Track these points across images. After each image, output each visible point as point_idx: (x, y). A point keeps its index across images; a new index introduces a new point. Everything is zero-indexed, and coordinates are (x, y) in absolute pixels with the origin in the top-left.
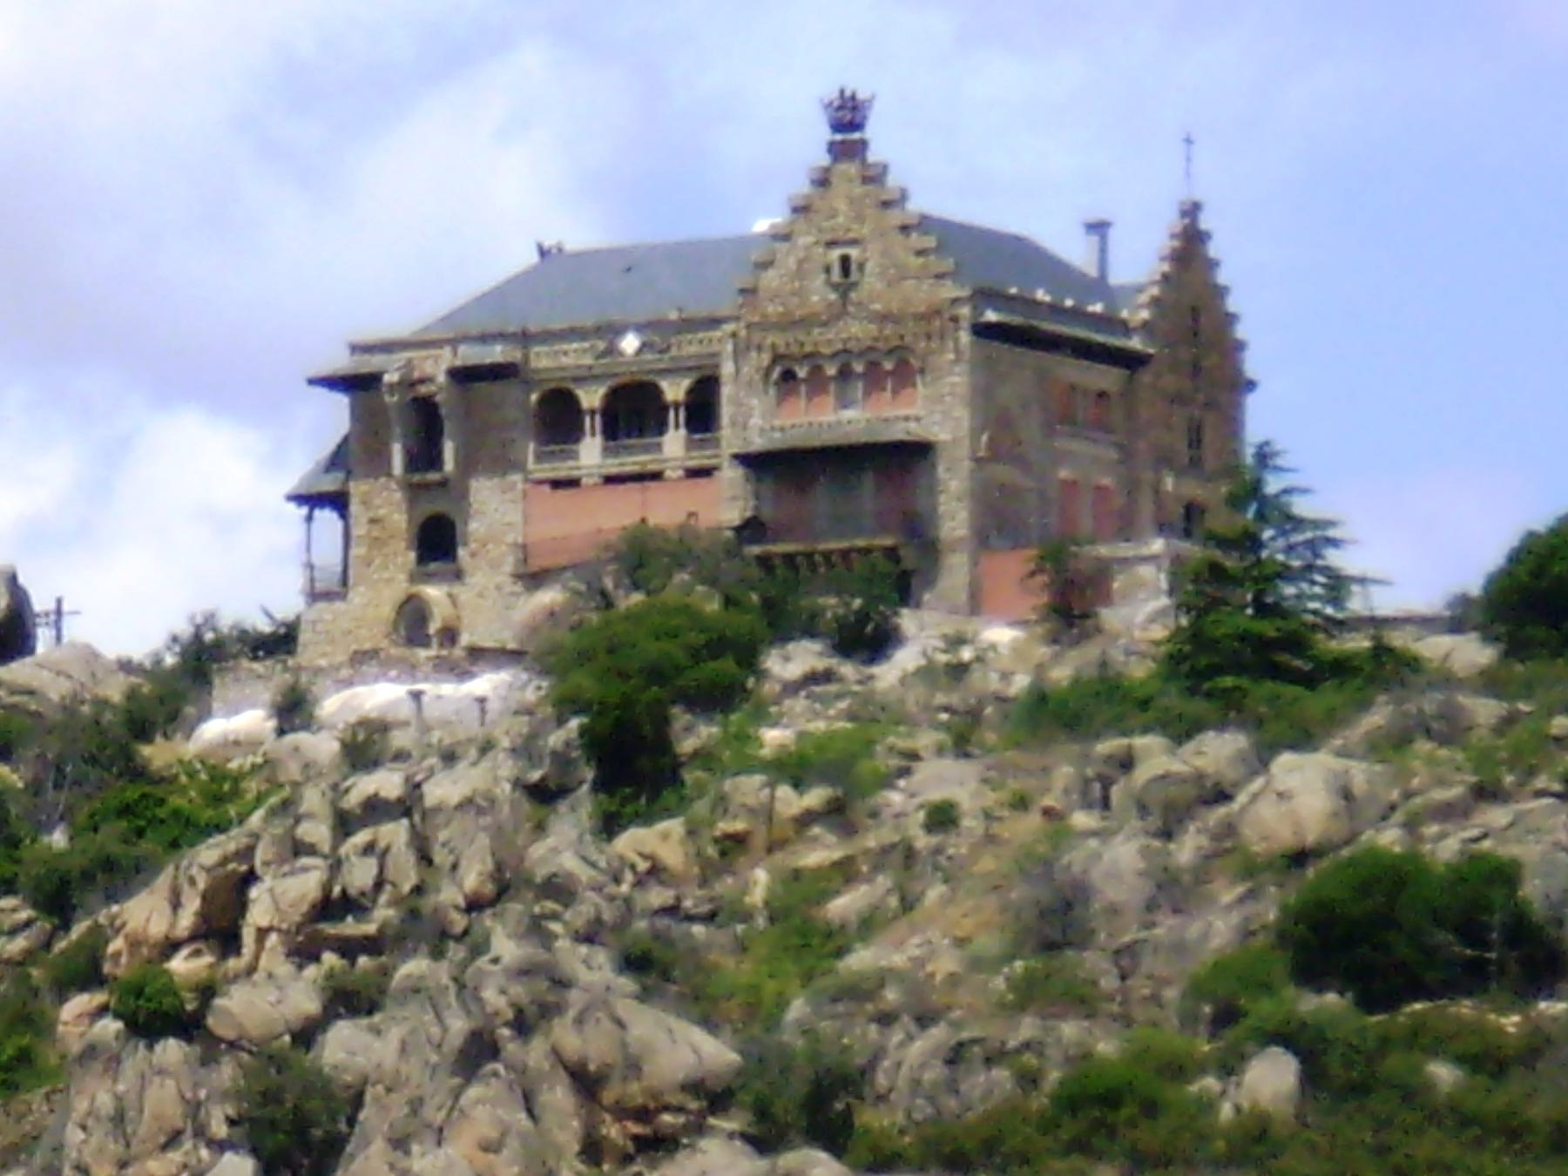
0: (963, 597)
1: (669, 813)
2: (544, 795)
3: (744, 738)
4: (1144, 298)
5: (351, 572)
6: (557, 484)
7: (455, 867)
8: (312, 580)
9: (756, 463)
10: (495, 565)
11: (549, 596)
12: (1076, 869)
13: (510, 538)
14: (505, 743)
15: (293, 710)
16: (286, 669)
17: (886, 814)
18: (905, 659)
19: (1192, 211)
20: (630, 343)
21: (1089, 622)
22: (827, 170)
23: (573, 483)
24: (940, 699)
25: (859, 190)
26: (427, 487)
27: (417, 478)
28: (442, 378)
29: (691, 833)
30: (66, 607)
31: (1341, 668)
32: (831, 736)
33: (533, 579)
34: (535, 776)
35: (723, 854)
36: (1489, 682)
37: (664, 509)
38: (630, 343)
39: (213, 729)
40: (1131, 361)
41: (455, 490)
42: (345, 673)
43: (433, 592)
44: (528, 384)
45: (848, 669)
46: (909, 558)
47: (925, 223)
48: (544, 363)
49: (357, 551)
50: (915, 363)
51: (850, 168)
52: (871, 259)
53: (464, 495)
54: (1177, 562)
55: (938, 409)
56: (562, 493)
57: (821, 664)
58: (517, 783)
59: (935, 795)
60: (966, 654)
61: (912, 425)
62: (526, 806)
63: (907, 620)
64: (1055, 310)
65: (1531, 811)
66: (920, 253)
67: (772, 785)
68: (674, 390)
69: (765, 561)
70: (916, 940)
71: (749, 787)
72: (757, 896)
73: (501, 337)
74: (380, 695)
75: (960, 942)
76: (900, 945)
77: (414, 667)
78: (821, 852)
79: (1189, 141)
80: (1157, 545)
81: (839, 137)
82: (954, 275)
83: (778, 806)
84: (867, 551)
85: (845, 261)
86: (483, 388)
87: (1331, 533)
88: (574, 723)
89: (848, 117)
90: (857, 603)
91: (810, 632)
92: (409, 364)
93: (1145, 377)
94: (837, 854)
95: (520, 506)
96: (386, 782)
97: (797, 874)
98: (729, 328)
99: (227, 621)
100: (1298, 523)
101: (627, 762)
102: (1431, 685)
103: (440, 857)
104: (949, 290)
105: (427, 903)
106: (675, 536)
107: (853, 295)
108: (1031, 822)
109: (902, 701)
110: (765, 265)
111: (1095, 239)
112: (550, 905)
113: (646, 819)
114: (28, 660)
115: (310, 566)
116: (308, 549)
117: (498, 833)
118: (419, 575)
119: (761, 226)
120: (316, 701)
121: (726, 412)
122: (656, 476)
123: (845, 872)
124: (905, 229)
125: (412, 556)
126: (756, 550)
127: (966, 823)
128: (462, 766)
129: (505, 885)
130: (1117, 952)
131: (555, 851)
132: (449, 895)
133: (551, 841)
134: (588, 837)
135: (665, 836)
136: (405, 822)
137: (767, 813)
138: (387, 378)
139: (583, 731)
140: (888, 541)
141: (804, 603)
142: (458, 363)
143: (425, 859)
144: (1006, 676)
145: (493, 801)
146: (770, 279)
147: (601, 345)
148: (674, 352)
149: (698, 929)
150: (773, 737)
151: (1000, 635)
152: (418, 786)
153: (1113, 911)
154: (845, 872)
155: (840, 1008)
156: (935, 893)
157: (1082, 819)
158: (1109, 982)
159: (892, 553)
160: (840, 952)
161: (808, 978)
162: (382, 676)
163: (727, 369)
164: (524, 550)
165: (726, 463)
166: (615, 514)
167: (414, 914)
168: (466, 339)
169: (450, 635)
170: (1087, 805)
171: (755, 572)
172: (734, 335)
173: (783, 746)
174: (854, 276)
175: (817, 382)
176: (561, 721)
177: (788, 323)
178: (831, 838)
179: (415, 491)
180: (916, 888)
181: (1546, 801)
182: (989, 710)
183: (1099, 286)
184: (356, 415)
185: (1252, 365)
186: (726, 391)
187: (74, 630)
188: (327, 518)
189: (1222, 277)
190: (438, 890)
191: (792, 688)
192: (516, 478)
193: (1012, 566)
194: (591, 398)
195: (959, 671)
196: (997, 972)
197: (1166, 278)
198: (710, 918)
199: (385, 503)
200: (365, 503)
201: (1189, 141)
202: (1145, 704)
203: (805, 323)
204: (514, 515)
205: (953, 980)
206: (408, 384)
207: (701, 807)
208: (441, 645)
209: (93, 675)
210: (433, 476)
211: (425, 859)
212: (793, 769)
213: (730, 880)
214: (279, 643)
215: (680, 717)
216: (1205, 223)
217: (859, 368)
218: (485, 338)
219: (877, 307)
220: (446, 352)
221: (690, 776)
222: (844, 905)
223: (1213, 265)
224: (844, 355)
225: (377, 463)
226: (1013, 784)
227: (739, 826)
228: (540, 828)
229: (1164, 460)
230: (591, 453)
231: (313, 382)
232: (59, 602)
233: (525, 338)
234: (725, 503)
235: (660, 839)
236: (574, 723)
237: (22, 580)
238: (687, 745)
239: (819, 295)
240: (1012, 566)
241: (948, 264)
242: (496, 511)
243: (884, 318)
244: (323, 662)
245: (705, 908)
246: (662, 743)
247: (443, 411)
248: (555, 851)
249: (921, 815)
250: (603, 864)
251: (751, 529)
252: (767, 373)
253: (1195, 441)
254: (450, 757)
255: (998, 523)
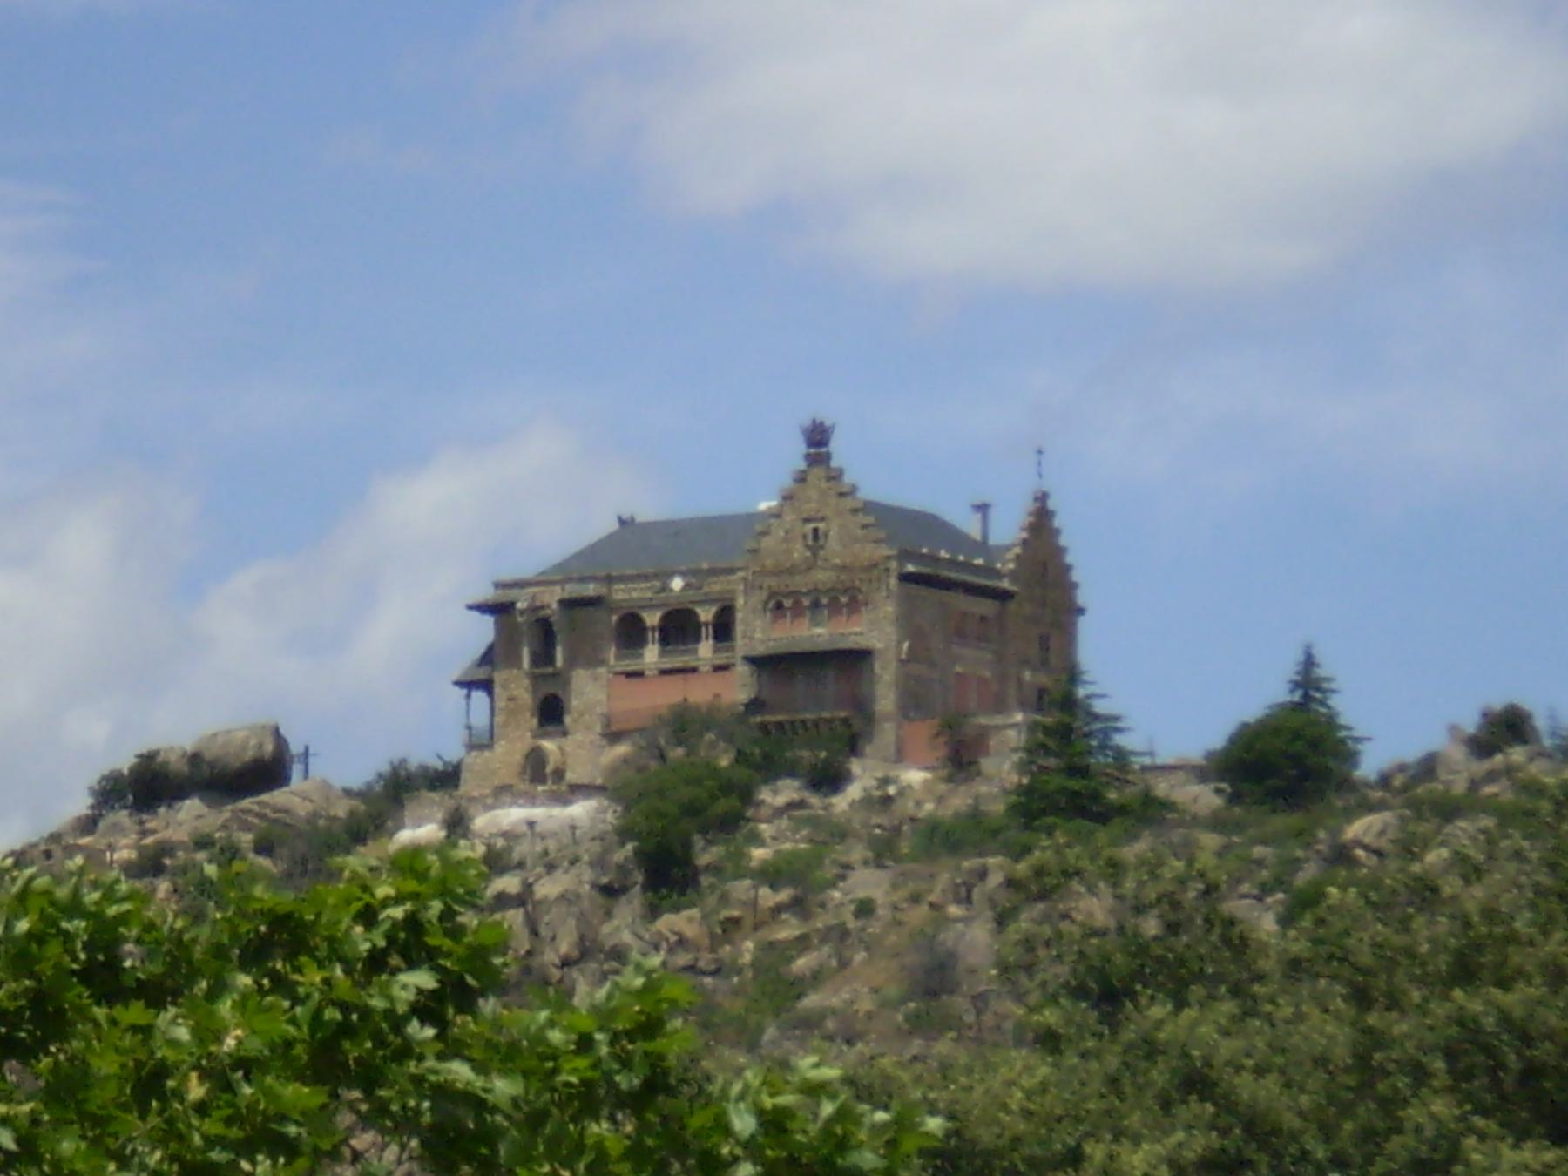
0: (892, 750)
1: (692, 905)
2: (611, 892)
3: (739, 856)
4: (1010, 555)
5: (496, 731)
6: (629, 675)
7: (553, 938)
8: (470, 735)
9: (759, 663)
10: (588, 728)
11: (622, 749)
12: (950, 944)
13: (599, 710)
14: (586, 858)
15: (457, 824)
16: (451, 796)
17: (830, 905)
18: (854, 791)
19: (1042, 498)
20: (677, 584)
21: (973, 768)
22: (803, 472)
23: (638, 675)
24: (875, 820)
25: (824, 485)
26: (544, 676)
27: (538, 671)
28: (554, 606)
29: (704, 917)
30: (311, 751)
31: (1122, 810)
32: (795, 854)
33: (613, 737)
34: (604, 880)
35: (724, 931)
36: (1216, 823)
37: (699, 692)
38: (677, 584)
39: (406, 836)
40: (1003, 596)
41: (561, 678)
42: (490, 801)
43: (548, 745)
44: (612, 610)
45: (814, 800)
46: (857, 724)
47: (869, 507)
48: (619, 596)
49: (498, 719)
50: (860, 597)
51: (818, 471)
52: (833, 530)
53: (566, 683)
54: (1032, 727)
55: (876, 629)
56: (635, 681)
57: (795, 796)
58: (594, 885)
59: (861, 894)
60: (892, 790)
61: (858, 638)
62: (600, 899)
63: (855, 766)
64: (952, 563)
66: (865, 527)
67: (755, 887)
68: (706, 614)
69: (764, 727)
70: (847, 988)
71: (741, 888)
72: (747, 958)
73: (593, 579)
74: (512, 815)
75: (876, 991)
76: (836, 991)
77: (534, 797)
78: (788, 930)
79: (1040, 452)
80: (1019, 717)
81: (812, 451)
82: (887, 541)
83: (761, 902)
84: (829, 721)
85: (816, 530)
86: (581, 613)
87: (1119, 724)
88: (630, 847)
89: (818, 437)
90: (823, 754)
91: (792, 774)
92: (534, 597)
93: (1012, 606)
94: (797, 933)
96: (509, 883)
97: (772, 945)
98: (741, 574)
99: (414, 763)
100: (1097, 717)
101: (664, 871)
102: (1181, 824)
103: (544, 932)
104: (885, 551)
105: (535, 962)
106: (704, 710)
107: (822, 553)
108: (924, 909)
109: (849, 820)
110: (764, 533)
111: (979, 516)
112: (614, 964)
113: (676, 909)
114: (285, 789)
115: (469, 728)
116: (468, 712)
117: (582, 917)
118: (541, 733)
119: (763, 506)
120: (471, 819)
121: (739, 629)
122: (694, 670)
123: (802, 943)
124: (855, 511)
125: (535, 722)
126: (758, 719)
127: (880, 912)
128: (558, 873)
129: (586, 950)
130: (973, 997)
131: (618, 929)
132: (550, 957)
133: (616, 922)
134: (638, 920)
135: (690, 920)
136: (521, 911)
137: (754, 904)
138: (519, 605)
139: (637, 852)
140: (843, 714)
141: (788, 754)
142: (566, 595)
143: (535, 933)
144: (919, 804)
145: (578, 896)
146: (767, 543)
147: (658, 584)
148: (706, 589)
149: (708, 980)
150: (759, 854)
151: (914, 776)
152: (530, 885)
153: (972, 971)
154: (802, 943)
155: (798, 1032)
156: (860, 957)
157: (954, 910)
158: (970, 1018)
159: (846, 722)
160: (799, 997)
161: (777, 1013)
162: (513, 804)
163: (740, 601)
164: (608, 720)
165: (739, 661)
166: (667, 695)
167: (527, 970)
168: (570, 580)
169: (559, 774)
170: (958, 901)
171: (758, 734)
172: (745, 579)
173: (765, 861)
174: (821, 541)
175: (798, 611)
176: (623, 844)
177: (778, 572)
178: (794, 921)
179: (536, 679)
180: (847, 954)
181: (1247, 901)
182: (905, 828)
183: (982, 546)
184: (499, 628)
185: (1083, 597)
186: (739, 616)
187: (318, 768)
188: (479, 696)
189: (1063, 540)
190: (542, 953)
191: (780, 812)
192: (602, 670)
193: (922, 730)
194: (652, 619)
195: (887, 800)
196: (896, 1010)
197: (1025, 542)
198: (715, 973)
199: (517, 685)
200: (504, 687)
201: (1040, 452)
202: (995, 833)
203: (792, 571)
204: (602, 697)
205: (870, 1016)
206: (534, 609)
207: (711, 900)
209: (328, 798)
210: (550, 670)
211: (535, 933)
212: (771, 875)
213: (728, 948)
214: (446, 778)
215: (698, 841)
216: (1051, 504)
217: (825, 601)
218: (583, 580)
219: (837, 561)
220: (558, 589)
221: (705, 881)
222: (802, 964)
223: (1057, 532)
224: (815, 592)
225: (513, 660)
226: (911, 886)
227: (736, 913)
228: (608, 914)
229: (1026, 663)
230: (651, 655)
231: (470, 607)
232: (307, 749)
233: (609, 580)
234: (738, 688)
235: (682, 922)
236: (630, 847)
237: (283, 731)
238: (703, 859)
239: (799, 552)
240: (922, 730)
241: (882, 535)
242: (589, 692)
243: (844, 568)
244: (475, 794)
245: (713, 967)
246: (686, 861)
247: (555, 628)
248: (618, 929)
249: (852, 907)
250: (647, 937)
251: (755, 705)
252: (766, 603)
253: (1044, 642)
254: (551, 867)
255: (913, 703)
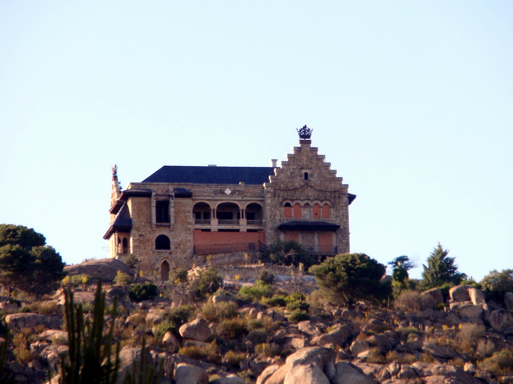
56: (204, 233)
65: (434, 287)
89: (305, 135)
95: (192, 235)
208: (240, 287)
